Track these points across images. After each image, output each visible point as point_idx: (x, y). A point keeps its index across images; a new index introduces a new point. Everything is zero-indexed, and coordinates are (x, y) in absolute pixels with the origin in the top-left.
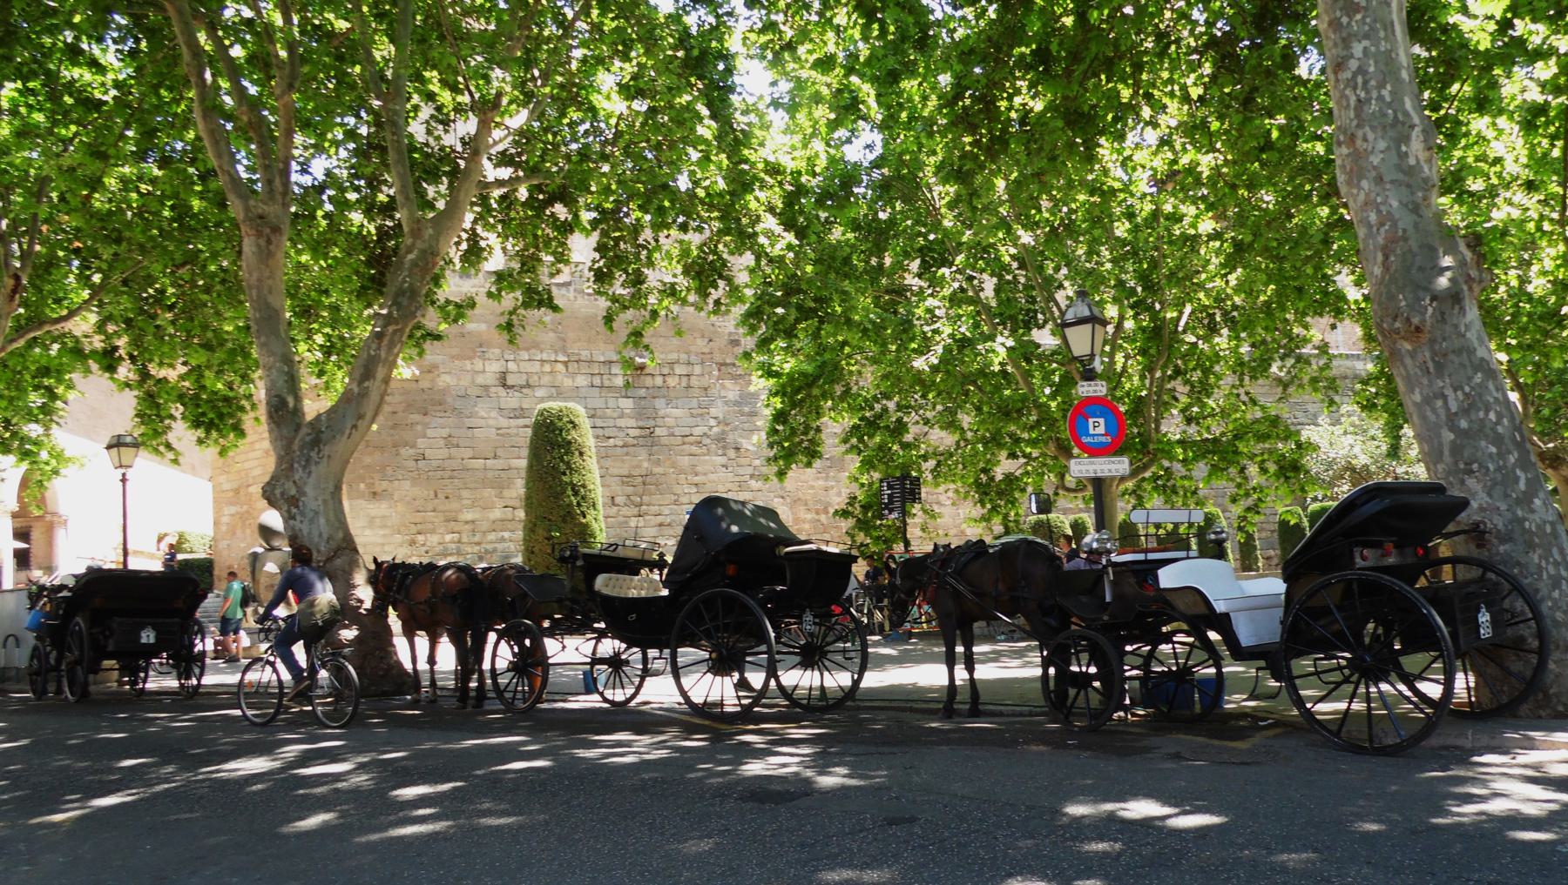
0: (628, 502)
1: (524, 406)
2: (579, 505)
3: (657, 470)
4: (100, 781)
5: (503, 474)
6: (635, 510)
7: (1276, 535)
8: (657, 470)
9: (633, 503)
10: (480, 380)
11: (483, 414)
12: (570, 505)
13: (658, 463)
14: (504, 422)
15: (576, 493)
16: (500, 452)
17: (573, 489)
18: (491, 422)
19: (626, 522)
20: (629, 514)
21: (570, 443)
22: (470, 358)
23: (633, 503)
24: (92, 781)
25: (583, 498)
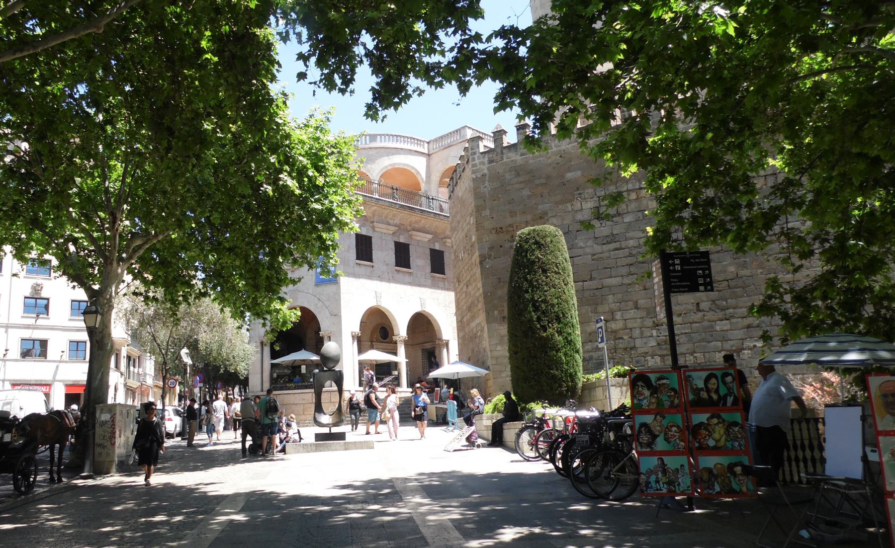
0: (713, 307)
1: (615, 232)
2: (539, 319)
3: (744, 272)
4: (149, 492)
5: (597, 292)
6: (721, 315)
7: (668, 337)
8: (744, 272)
9: (718, 307)
10: (579, 217)
11: (582, 244)
12: (531, 320)
13: (744, 266)
14: (598, 248)
15: (536, 309)
16: (594, 275)
17: (534, 305)
18: (588, 250)
19: (712, 327)
20: (715, 317)
21: (534, 262)
22: (571, 201)
23: (718, 307)
24: (118, 491)
25: (543, 313)
